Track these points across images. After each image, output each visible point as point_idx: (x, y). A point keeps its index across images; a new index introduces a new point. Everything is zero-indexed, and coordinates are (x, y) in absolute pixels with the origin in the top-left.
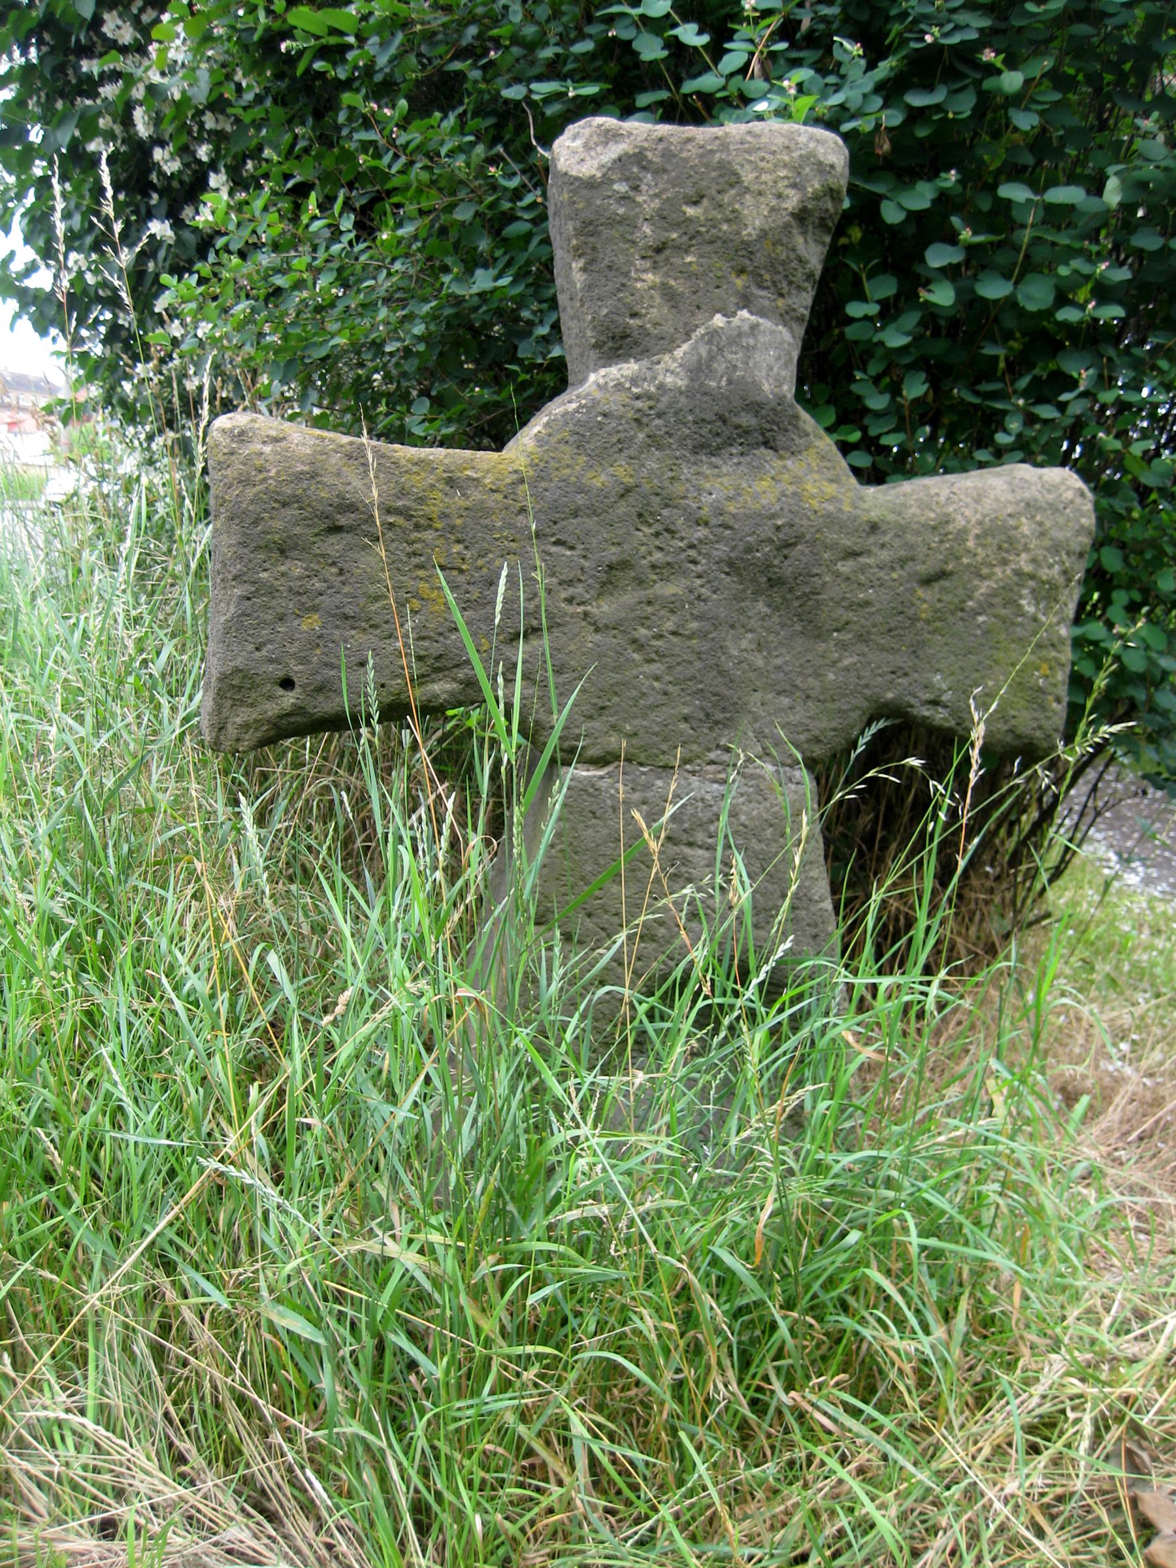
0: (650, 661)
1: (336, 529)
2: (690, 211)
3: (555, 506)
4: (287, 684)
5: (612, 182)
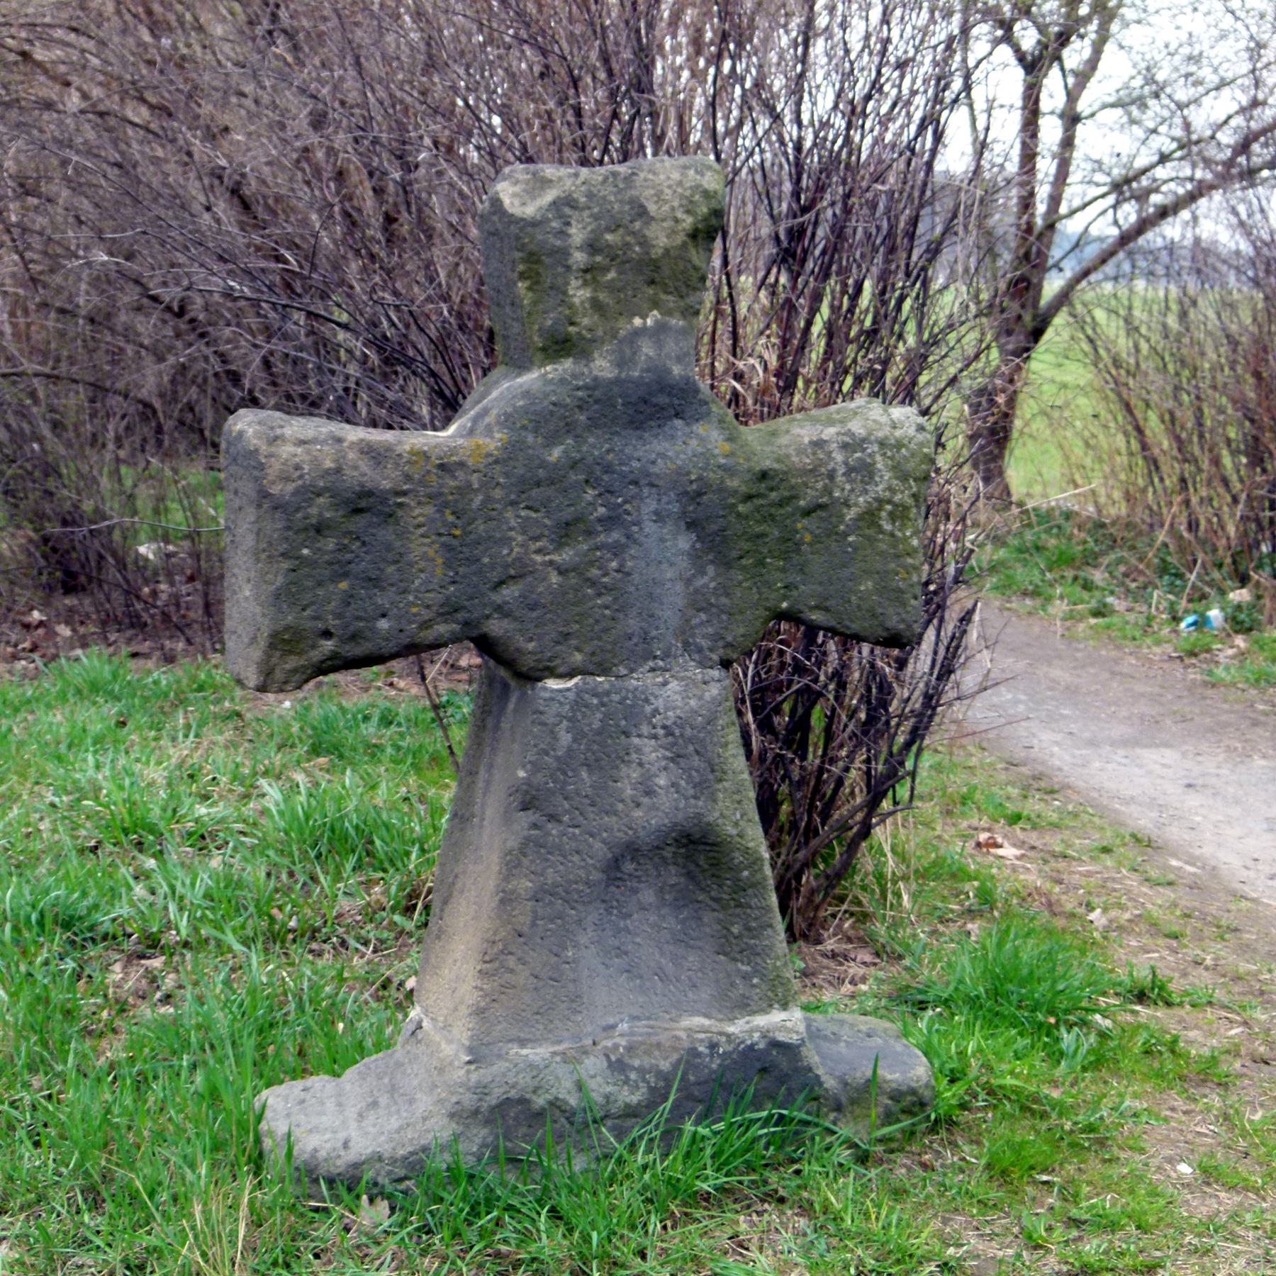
0: (599, 595)
1: (358, 511)
2: (609, 237)
3: (522, 480)
4: (327, 634)
5: (549, 220)
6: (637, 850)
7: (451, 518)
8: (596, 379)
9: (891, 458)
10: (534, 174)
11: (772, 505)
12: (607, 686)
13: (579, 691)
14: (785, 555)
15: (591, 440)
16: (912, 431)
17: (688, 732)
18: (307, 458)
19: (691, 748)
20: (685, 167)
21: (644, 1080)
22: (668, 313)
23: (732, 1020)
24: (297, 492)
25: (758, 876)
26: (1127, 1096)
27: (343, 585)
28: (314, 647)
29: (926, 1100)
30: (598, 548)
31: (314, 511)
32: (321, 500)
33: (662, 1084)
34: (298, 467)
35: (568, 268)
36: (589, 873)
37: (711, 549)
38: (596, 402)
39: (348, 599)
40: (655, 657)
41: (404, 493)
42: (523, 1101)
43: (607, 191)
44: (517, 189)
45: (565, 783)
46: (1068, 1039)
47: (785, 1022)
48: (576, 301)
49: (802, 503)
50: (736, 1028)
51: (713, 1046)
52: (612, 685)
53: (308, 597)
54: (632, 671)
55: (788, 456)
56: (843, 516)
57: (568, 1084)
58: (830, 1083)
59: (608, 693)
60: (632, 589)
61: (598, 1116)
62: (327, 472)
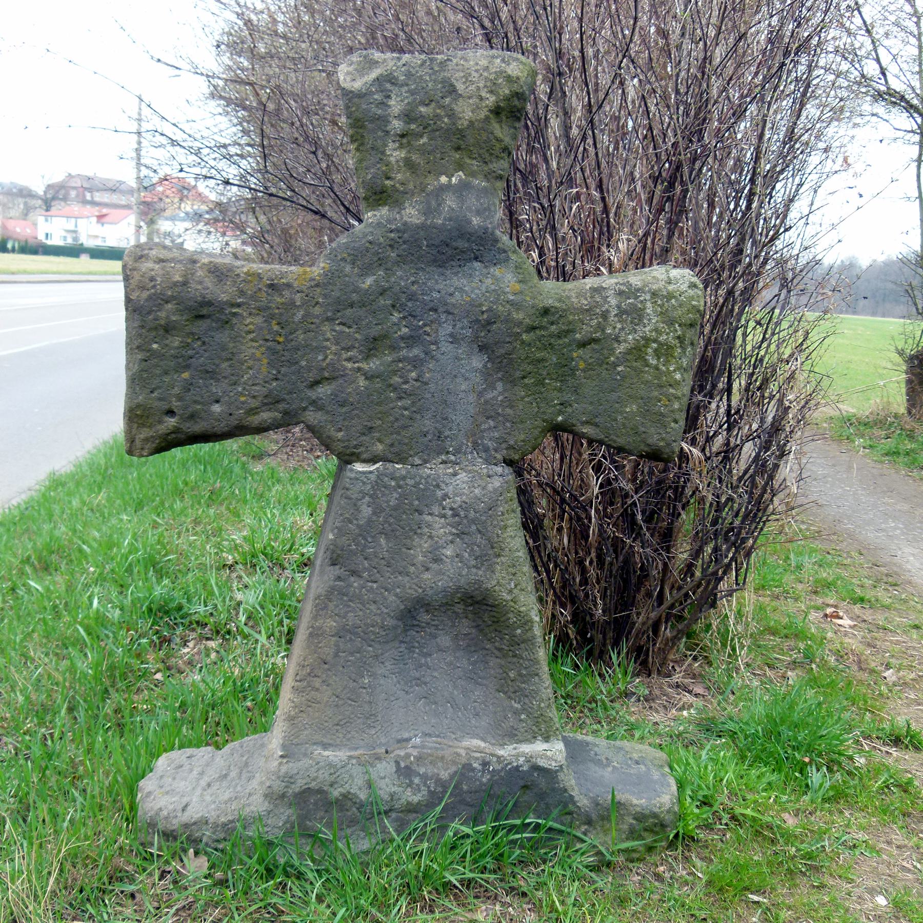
0: (400, 398)
2: (423, 109)
3: (338, 301)
4: (171, 413)
6: (428, 604)
7: (276, 328)
8: (405, 224)
9: (661, 306)
10: (365, 57)
11: (551, 336)
12: (404, 472)
13: (380, 475)
14: (562, 379)
15: (399, 273)
16: (684, 287)
17: (472, 514)
18: (161, 272)
19: (474, 527)
20: (493, 57)
21: (425, 784)
22: (473, 174)
23: (502, 745)
24: (150, 298)
25: (529, 634)
26: (853, 825)
27: (186, 375)
28: (160, 422)
29: (667, 822)
30: (400, 361)
31: (162, 314)
32: (170, 306)
33: (439, 789)
34: (152, 279)
35: (387, 133)
36: (383, 620)
37: (499, 369)
38: (404, 242)
39: (188, 386)
40: (448, 453)
41: (239, 305)
42: (320, 791)
43: (424, 72)
44: (351, 69)
45: (365, 546)
46: (815, 777)
47: (549, 752)
48: (392, 159)
49: (578, 336)
50: (506, 752)
51: (485, 764)
52: (409, 472)
53: (156, 382)
54: (426, 462)
55: (569, 298)
56: (613, 349)
57: (360, 781)
58: (583, 802)
59: (404, 478)
60: (428, 396)
61: (383, 808)
62: (175, 284)
